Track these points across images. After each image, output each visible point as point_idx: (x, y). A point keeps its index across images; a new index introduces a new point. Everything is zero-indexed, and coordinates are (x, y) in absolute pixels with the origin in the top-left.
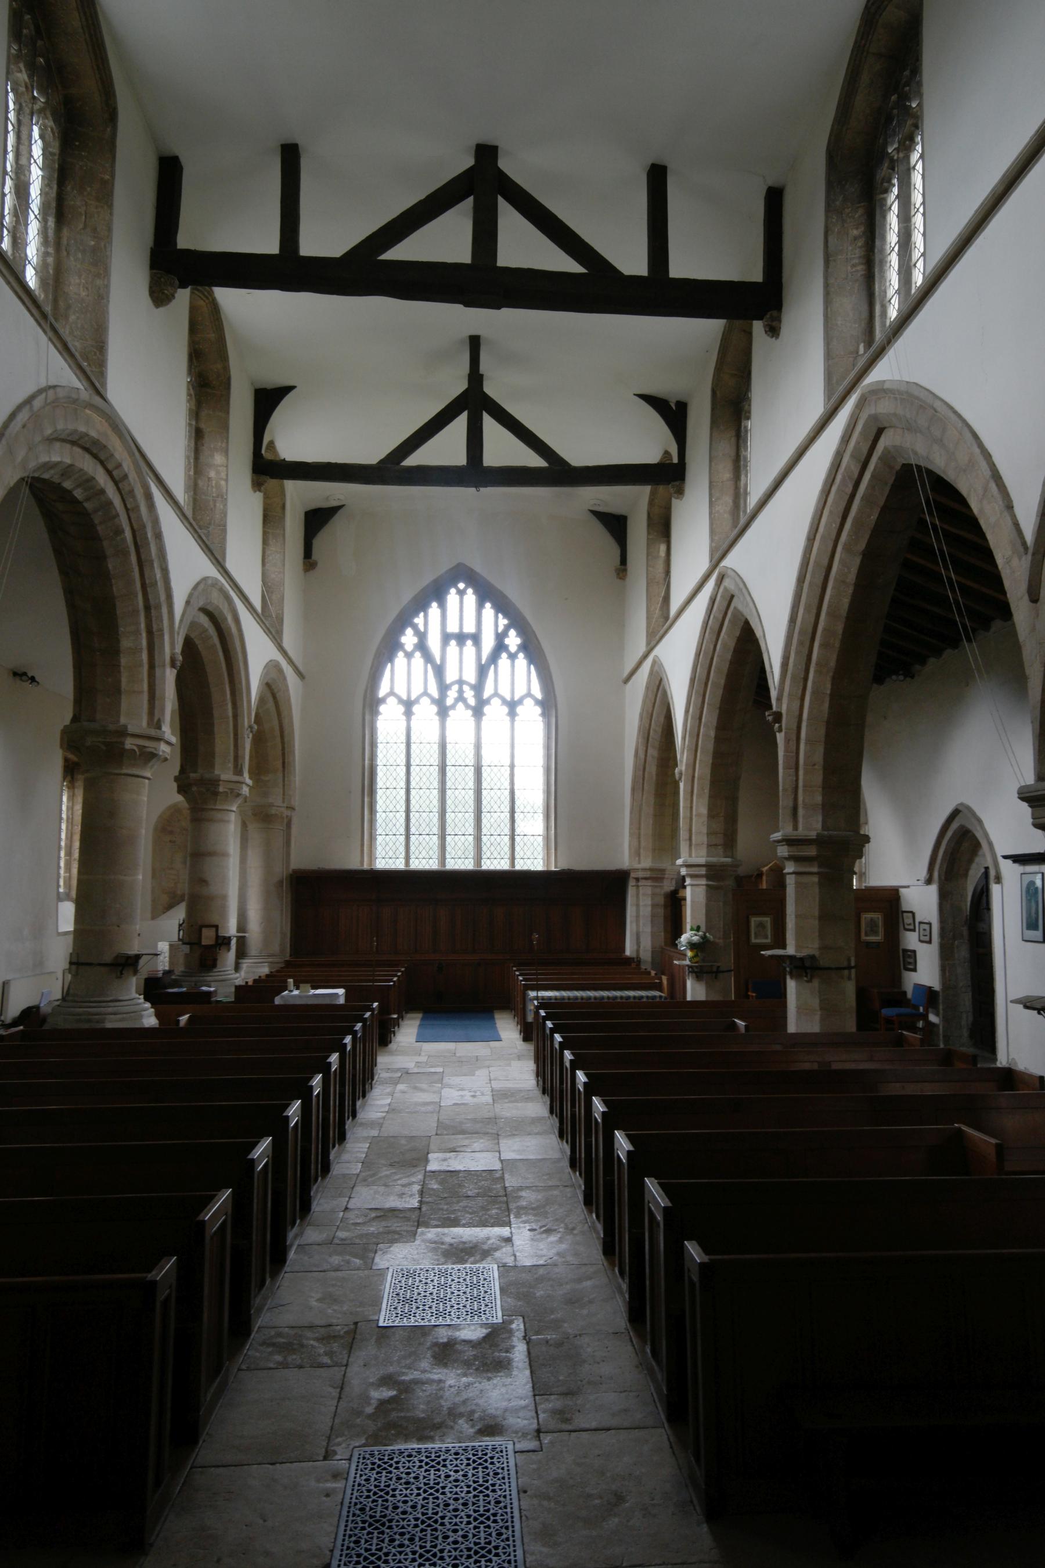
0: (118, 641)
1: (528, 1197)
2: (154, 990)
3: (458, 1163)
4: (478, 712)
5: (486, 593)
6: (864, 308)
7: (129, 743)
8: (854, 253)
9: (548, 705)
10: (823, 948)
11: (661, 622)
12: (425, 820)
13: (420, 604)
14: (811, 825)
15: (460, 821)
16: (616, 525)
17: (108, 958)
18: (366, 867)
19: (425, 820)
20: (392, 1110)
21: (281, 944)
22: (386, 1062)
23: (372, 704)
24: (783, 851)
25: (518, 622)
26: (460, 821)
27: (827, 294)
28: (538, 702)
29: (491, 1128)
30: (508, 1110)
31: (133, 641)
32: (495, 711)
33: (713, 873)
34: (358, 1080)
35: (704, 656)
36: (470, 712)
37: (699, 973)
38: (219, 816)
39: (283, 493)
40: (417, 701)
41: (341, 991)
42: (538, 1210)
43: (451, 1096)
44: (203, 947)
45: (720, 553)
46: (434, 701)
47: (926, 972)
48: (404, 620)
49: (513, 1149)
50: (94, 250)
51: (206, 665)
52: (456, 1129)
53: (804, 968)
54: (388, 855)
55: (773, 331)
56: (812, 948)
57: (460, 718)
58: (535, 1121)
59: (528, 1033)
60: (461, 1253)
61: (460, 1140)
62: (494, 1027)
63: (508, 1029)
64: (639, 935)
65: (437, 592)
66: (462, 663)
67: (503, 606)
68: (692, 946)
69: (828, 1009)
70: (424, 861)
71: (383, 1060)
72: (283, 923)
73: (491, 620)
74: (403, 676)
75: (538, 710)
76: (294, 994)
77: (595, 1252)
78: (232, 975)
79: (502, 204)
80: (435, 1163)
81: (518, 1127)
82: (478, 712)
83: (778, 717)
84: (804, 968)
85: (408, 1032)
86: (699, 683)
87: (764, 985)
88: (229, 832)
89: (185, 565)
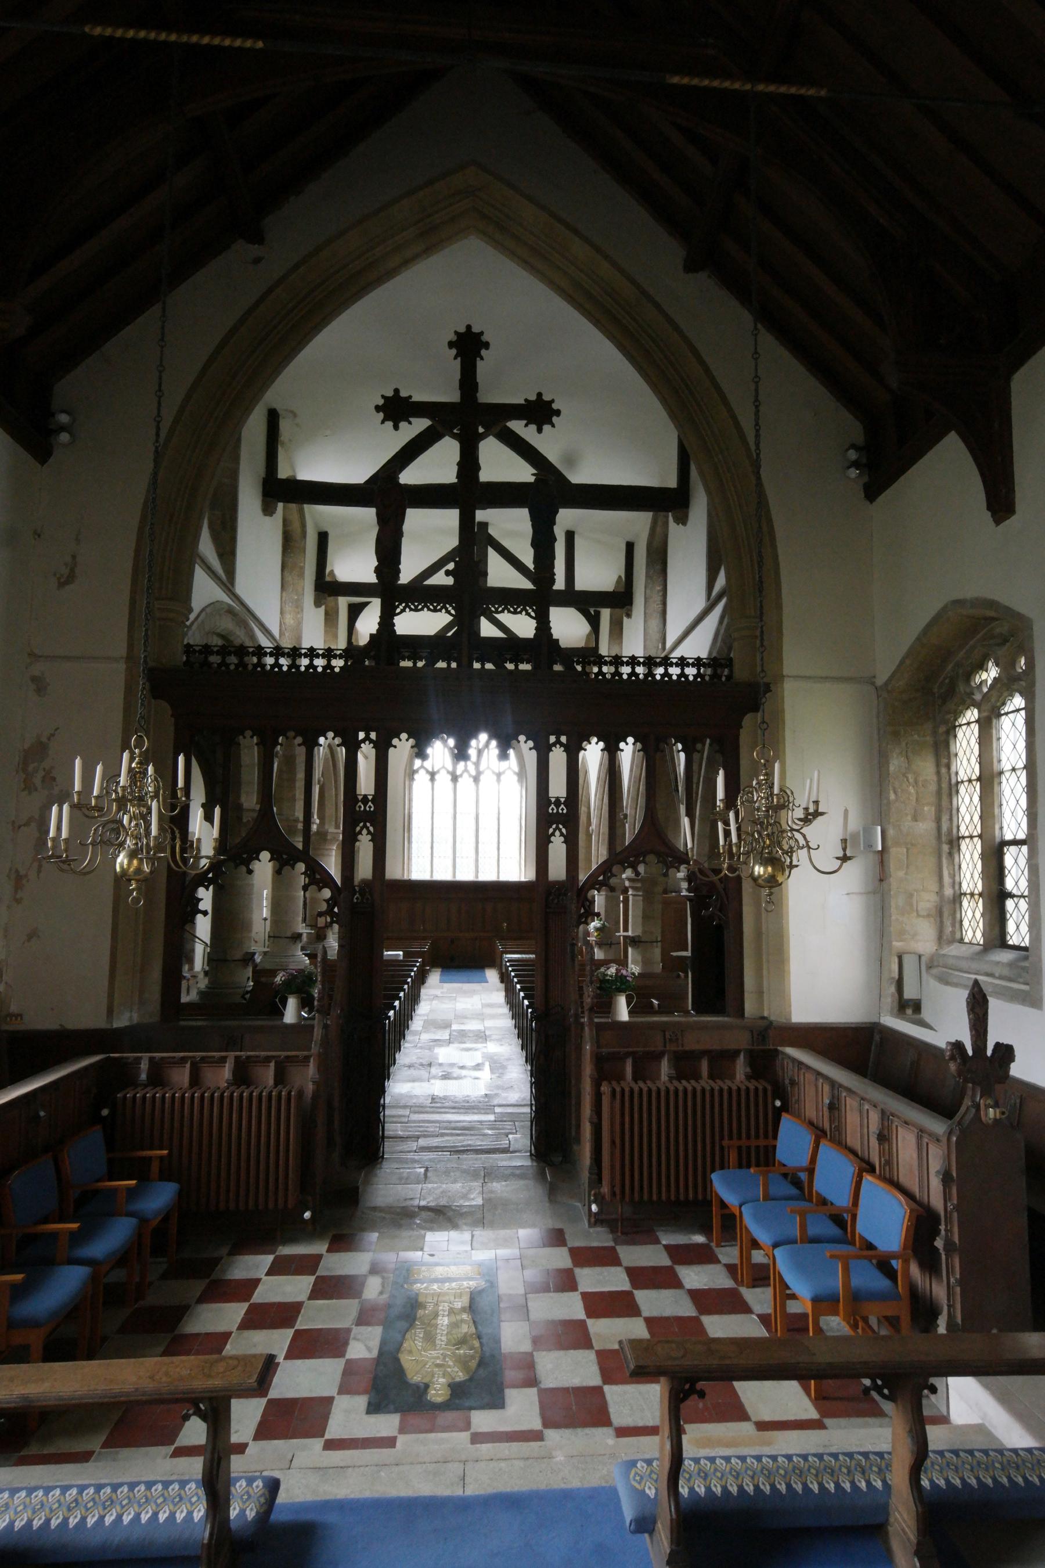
0: (295, 775)
4: (476, 779)
6: (661, 626)
7: (792, 1143)
8: (658, 598)
10: (644, 932)
12: (443, 849)
17: (289, 934)
18: (406, 878)
20: (431, 1011)
22: (424, 992)
24: (627, 884)
27: (645, 621)
28: (515, 773)
34: (414, 999)
36: (472, 780)
37: (600, 945)
38: (326, 852)
39: (337, 604)
40: (438, 771)
41: (401, 953)
46: (448, 772)
50: (298, 600)
53: (634, 941)
55: (629, 616)
56: (639, 932)
58: (505, 1014)
59: (504, 978)
61: (465, 1021)
62: (485, 977)
63: (492, 975)
68: (597, 929)
69: (646, 962)
71: (423, 991)
75: (516, 778)
79: (490, 550)
80: (454, 1027)
82: (476, 779)
83: (626, 816)
85: (434, 977)
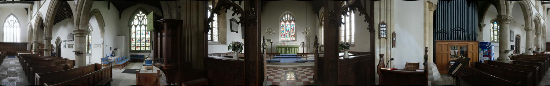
1: (19, 74)
2: (534, 52)
3: (11, 70)
5: (14, 16)
9: (20, 27)
11: (31, 18)
12: (8, 38)
13: (8, 17)
14: (47, 36)
15: (12, 38)
16: (27, 9)
19: (8, 38)
21: (545, 49)
23: (3, 27)
25: (17, 19)
26: (12, 38)
29: (14, 66)
30: (16, 64)
31: (529, 19)
32: (15, 27)
33: (36, 42)
35: (36, 21)
42: (20, 75)
43: (11, 63)
44: (538, 49)
45: (38, 10)
47: (55, 51)
48: (6, 19)
49: (17, 68)
51: (537, 22)
52: (11, 66)
53: (46, 50)
54: (5, 41)
57: (12, 28)
59: (18, 57)
60: (12, 80)
63: (16, 57)
64: (28, 48)
65: (9, 16)
66: (12, 23)
67: (16, 17)
70: (8, 42)
72: (545, 47)
73: (15, 19)
74: (6, 24)
76: (546, 53)
77: (27, 80)
78: (540, 51)
81: (17, 66)
84: (46, 50)
85: (7, 57)
86: (35, 24)
87: (41, 52)
88: (540, 38)
89: (534, 12)
